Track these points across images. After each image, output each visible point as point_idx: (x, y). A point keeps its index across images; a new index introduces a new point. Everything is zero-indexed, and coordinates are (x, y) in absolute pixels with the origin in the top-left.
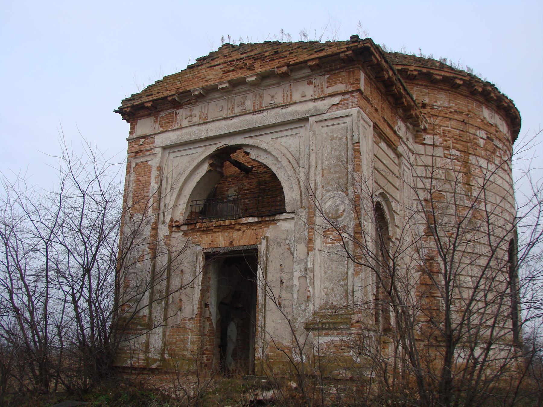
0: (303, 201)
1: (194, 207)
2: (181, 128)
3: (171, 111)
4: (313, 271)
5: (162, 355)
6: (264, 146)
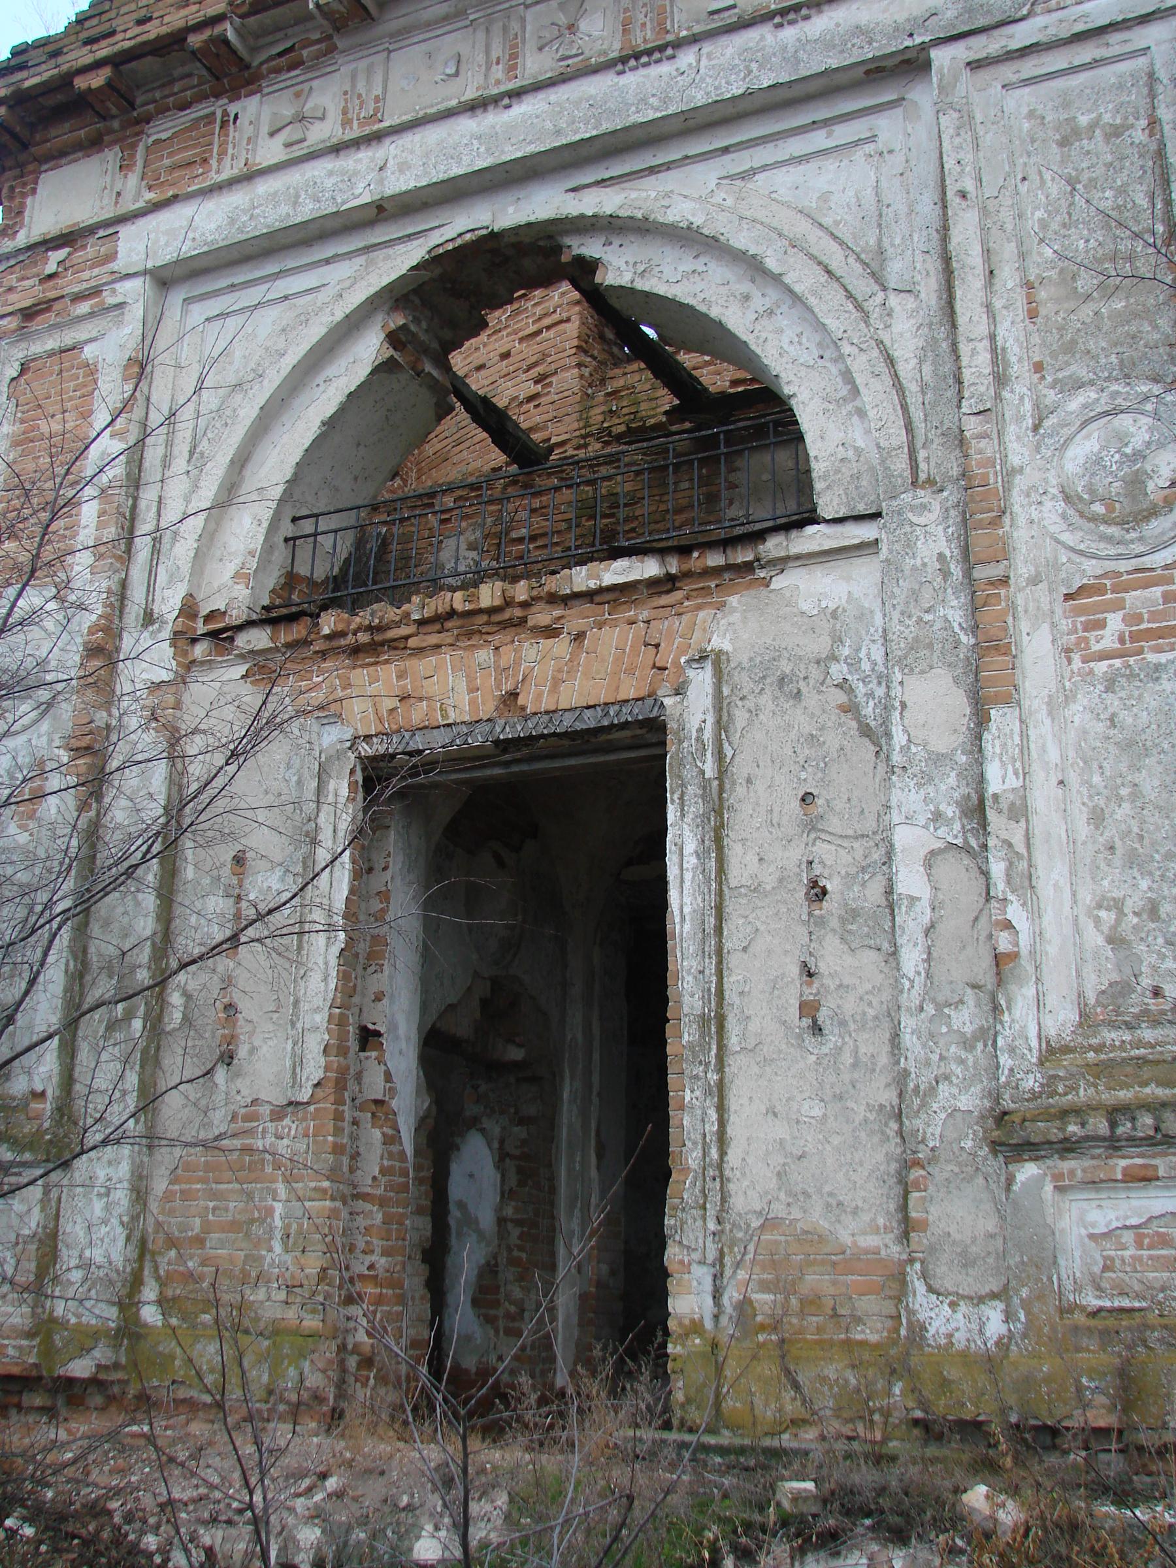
0: (922, 455)
1: (305, 548)
2: (249, 176)
3: (200, 110)
4: (1019, 811)
5: (128, 1304)
6: (680, 212)
